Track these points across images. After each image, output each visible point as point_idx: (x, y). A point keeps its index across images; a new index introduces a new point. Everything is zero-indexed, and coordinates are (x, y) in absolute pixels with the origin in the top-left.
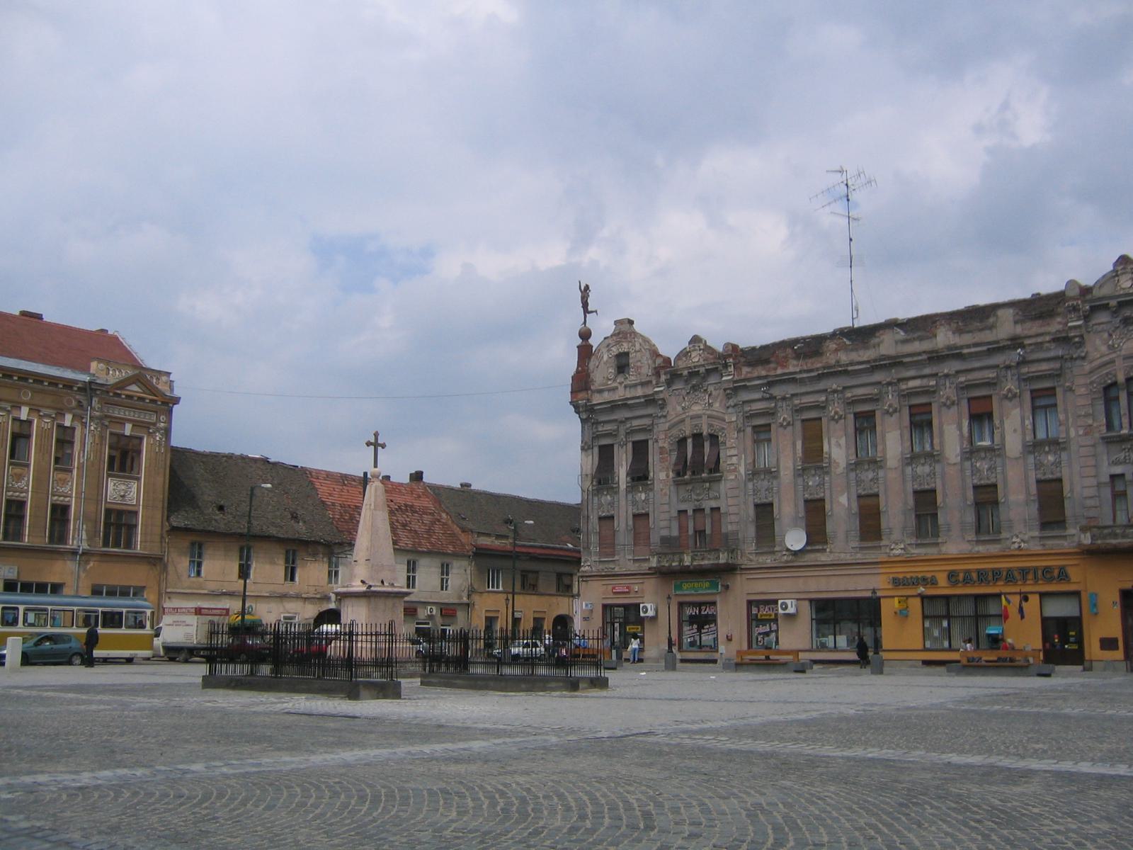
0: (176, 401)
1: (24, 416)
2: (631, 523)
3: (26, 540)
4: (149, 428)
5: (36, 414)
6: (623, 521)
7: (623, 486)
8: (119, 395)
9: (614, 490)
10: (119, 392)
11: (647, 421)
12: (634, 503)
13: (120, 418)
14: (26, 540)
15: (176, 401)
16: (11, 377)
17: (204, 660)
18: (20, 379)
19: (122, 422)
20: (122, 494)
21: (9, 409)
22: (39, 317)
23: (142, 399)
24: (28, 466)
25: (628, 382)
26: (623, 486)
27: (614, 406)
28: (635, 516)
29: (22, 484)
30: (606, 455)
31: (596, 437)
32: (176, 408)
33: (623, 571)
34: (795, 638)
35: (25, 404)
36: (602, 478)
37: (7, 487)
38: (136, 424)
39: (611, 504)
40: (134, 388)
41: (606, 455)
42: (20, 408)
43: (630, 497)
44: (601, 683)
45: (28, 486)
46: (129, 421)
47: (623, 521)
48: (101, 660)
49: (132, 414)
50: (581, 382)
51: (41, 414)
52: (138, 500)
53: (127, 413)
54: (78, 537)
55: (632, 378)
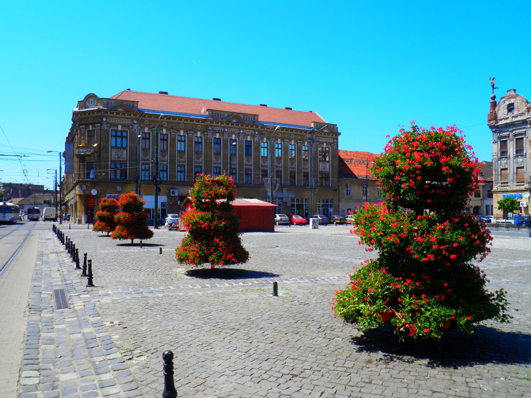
0: (340, 134)
1: (249, 139)
2: (515, 170)
6: (511, 171)
7: (512, 156)
9: (507, 158)
11: (524, 130)
12: (517, 163)
15: (340, 134)
25: (514, 115)
26: (512, 156)
27: (507, 125)
28: (517, 168)
29: (183, 159)
30: (504, 144)
31: (500, 138)
32: (339, 137)
33: (512, 189)
35: (182, 129)
36: (503, 153)
38: (123, 125)
39: (506, 163)
41: (504, 144)
43: (515, 160)
44: (77, 250)
46: (325, 142)
47: (511, 171)
50: (493, 117)
54: (312, 181)
55: (516, 112)
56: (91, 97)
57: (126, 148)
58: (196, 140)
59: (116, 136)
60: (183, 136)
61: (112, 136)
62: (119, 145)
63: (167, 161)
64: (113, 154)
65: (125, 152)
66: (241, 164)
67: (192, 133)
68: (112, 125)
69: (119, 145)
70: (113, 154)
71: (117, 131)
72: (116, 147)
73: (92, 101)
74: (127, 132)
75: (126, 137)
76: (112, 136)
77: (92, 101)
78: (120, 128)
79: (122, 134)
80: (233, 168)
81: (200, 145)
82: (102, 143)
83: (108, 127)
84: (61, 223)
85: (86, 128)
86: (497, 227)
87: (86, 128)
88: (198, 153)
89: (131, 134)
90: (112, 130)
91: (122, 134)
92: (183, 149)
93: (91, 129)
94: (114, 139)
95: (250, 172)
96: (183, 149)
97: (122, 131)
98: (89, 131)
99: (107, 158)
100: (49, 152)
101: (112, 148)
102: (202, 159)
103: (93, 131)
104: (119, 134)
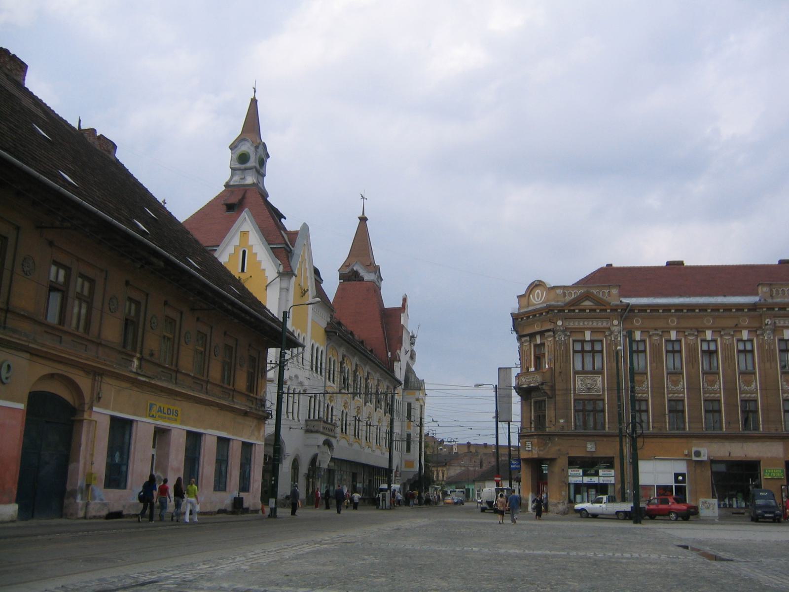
3: (761, 429)
4: (684, 332)
5: (681, 334)
8: (574, 311)
10: (572, 308)
13: (602, 328)
14: (761, 429)
16: (694, 310)
17: (772, 520)
18: (737, 310)
19: (582, 331)
20: (589, 386)
21: (732, 333)
22: (681, 263)
23: (594, 310)
24: (718, 374)
29: (716, 386)
34: (757, 482)
37: (703, 391)
38: (594, 331)
40: (587, 303)
42: (741, 331)
45: (648, 388)
46: (588, 329)
48: (384, 498)
49: (590, 323)
51: (686, 334)
52: (603, 390)
53: (586, 323)
56: (537, 285)
57: (600, 372)
58: (705, 347)
59: (583, 351)
60: (748, 340)
61: (575, 352)
62: (588, 367)
63: (684, 393)
64: (579, 384)
65: (599, 380)
66: (658, 389)
67: (729, 334)
68: (573, 331)
69: (588, 367)
70: (579, 384)
71: (583, 342)
72: (584, 372)
73: (538, 293)
74: (601, 341)
75: (601, 352)
76: (575, 352)
77: (538, 293)
78: (588, 336)
79: (593, 347)
80: (640, 401)
81: (715, 356)
82: (558, 365)
83: (566, 335)
84: (339, 512)
85: (530, 341)
86: (124, 587)
87: (530, 341)
88: (748, 374)
89: (608, 346)
90: (574, 341)
91: (593, 347)
92: (750, 368)
93: (539, 342)
94: (578, 357)
95: (680, 408)
96: (750, 368)
97: (592, 342)
98: (536, 346)
99: (567, 391)
100: (477, 386)
101: (576, 373)
102: (756, 384)
103: (543, 344)
104: (588, 347)
